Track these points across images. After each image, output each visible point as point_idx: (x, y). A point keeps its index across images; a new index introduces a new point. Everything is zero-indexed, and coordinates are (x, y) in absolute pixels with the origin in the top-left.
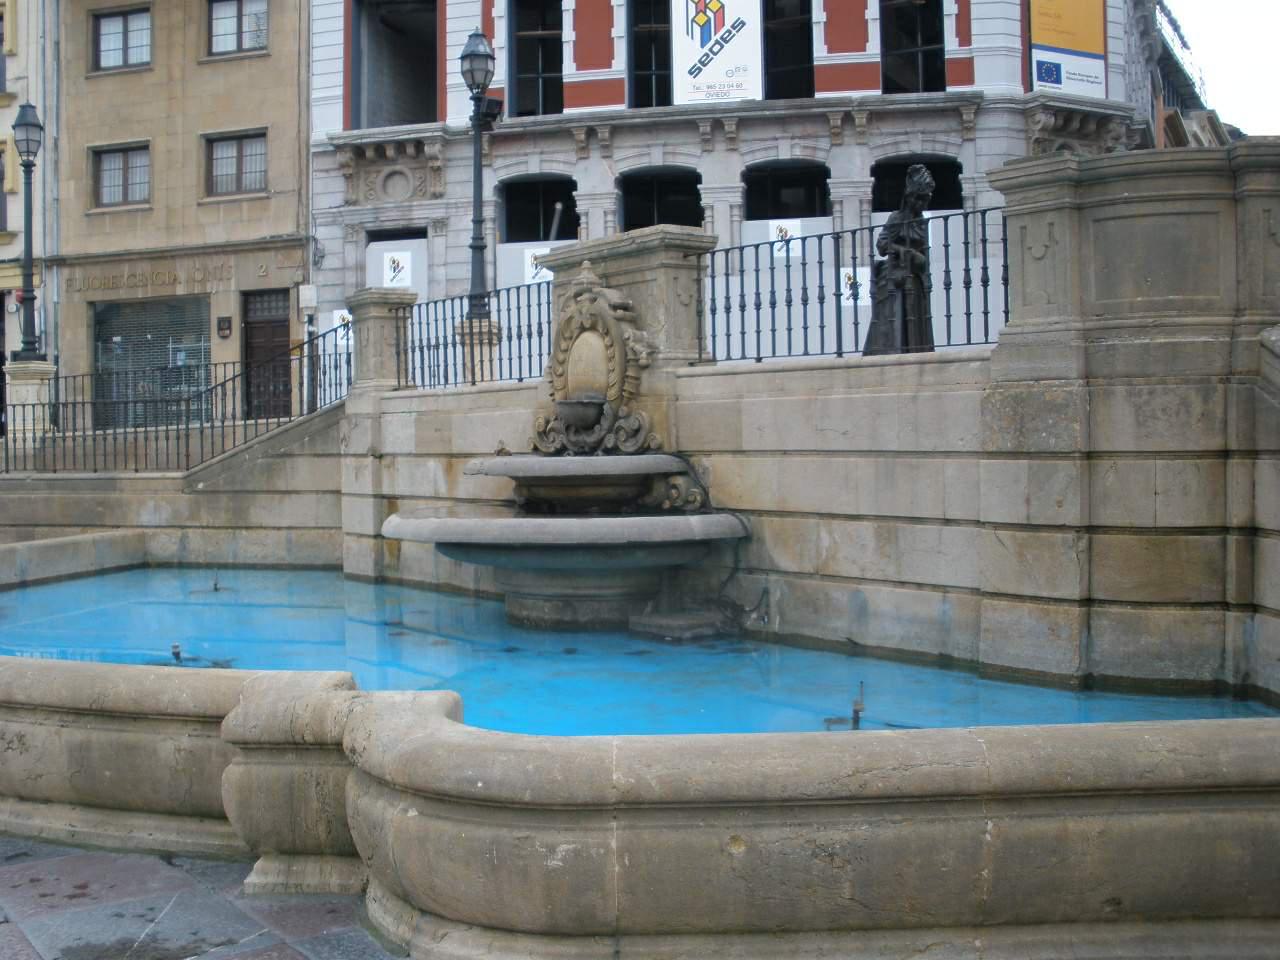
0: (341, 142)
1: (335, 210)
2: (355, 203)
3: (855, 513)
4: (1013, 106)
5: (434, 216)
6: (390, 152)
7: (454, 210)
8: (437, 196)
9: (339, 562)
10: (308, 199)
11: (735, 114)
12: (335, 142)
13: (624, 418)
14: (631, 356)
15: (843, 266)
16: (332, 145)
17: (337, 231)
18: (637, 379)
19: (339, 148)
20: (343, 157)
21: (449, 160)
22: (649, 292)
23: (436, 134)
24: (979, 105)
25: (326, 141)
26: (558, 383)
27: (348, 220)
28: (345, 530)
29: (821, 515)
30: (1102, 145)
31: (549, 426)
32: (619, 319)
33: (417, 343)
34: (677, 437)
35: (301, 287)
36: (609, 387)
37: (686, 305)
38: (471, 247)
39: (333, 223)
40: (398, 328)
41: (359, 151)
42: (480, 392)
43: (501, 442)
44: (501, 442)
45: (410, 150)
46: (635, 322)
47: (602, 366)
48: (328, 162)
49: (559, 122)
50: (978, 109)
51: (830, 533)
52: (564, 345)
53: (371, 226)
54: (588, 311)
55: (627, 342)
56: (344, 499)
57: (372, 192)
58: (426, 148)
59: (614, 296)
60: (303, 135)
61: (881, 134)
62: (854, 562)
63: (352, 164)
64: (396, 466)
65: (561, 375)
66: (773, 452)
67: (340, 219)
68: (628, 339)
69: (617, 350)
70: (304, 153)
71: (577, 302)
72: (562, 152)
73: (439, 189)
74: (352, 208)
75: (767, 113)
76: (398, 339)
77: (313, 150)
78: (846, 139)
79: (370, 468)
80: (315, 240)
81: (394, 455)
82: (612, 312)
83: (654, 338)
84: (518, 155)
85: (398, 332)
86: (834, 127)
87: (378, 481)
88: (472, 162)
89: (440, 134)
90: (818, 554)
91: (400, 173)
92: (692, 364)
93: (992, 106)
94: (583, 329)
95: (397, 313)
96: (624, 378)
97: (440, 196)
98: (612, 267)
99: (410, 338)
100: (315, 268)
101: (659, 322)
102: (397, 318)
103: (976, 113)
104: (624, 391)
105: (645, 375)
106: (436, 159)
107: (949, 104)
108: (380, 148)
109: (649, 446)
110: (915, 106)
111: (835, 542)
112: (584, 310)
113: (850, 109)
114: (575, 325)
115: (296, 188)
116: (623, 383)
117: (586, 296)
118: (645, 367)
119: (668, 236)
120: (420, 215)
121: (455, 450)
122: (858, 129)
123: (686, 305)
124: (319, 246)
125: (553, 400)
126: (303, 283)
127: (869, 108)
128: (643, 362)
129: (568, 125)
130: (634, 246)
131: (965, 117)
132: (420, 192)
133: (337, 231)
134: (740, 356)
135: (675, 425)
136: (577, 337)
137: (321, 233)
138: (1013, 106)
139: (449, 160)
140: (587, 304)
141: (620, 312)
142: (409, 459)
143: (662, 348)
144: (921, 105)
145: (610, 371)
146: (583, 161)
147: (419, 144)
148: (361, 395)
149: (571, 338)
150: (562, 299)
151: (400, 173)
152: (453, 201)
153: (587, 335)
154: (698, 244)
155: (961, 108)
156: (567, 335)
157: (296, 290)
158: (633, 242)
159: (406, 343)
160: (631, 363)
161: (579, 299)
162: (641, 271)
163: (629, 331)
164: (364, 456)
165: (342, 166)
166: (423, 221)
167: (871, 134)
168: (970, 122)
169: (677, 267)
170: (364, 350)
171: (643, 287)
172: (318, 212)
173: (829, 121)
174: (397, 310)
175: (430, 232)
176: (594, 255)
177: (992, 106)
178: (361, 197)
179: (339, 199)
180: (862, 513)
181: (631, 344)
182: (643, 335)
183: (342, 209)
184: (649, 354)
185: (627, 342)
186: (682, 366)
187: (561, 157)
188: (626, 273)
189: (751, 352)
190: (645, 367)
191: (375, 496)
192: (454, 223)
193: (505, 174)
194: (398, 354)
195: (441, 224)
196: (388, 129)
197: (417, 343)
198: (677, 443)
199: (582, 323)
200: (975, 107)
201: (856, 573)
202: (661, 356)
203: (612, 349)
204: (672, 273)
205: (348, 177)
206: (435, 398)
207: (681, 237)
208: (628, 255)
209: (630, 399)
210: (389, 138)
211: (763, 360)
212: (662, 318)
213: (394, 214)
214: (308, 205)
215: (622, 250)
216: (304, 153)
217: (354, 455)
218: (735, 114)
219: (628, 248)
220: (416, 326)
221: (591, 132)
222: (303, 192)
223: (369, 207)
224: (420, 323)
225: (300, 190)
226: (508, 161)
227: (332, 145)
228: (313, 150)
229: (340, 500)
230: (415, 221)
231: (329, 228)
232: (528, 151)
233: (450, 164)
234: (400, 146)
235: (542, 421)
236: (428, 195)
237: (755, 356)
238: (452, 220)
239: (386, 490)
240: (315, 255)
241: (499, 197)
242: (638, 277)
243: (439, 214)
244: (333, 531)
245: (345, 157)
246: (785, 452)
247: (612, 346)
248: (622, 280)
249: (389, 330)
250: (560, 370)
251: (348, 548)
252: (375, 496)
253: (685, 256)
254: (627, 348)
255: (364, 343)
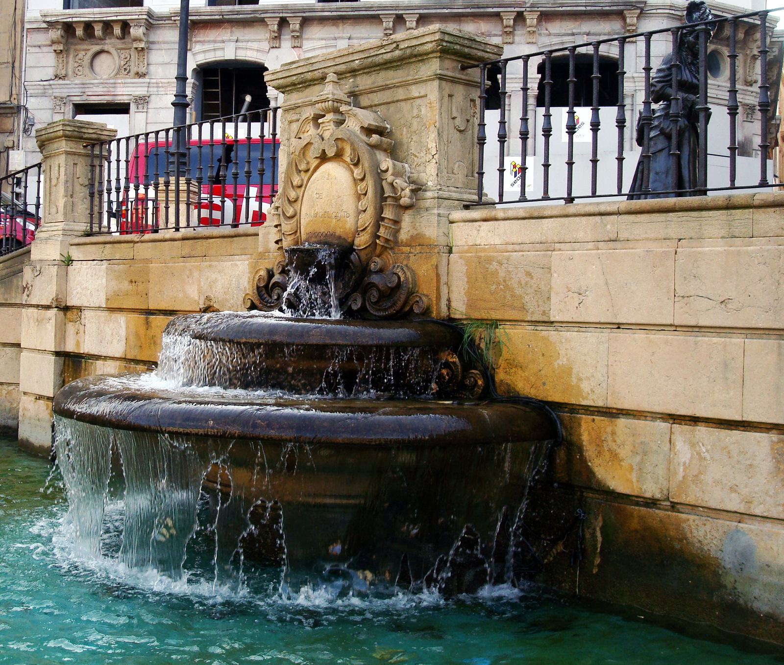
0: (53, 19)
1: (45, 83)
2: (64, 77)
3: (738, 418)
4: (673, 12)
5: (137, 93)
6: (98, 31)
7: (155, 89)
8: (140, 75)
9: (10, 423)
10: (21, 71)
11: (416, 11)
12: (48, 19)
13: (377, 272)
14: (388, 192)
15: (508, 155)
16: (45, 22)
17: (46, 103)
18: (396, 222)
19: (51, 25)
20: (55, 34)
21: (153, 43)
22: (415, 112)
23: (141, 17)
24: (642, 9)
25: (40, 18)
26: (287, 227)
27: (58, 92)
28: (22, 388)
29: (675, 418)
30: (748, 52)
31: (273, 281)
32: (374, 147)
33: (114, 184)
34: (449, 300)
35: (11, 152)
36: (357, 232)
37: (460, 131)
38: (173, 104)
39: (43, 95)
40: (93, 166)
41: (68, 28)
42: (184, 239)
43: (208, 298)
44: (208, 298)
45: (117, 30)
46: (393, 152)
47: (349, 205)
48: (42, 38)
49: (255, 11)
50: (641, 13)
51: (693, 445)
52: (296, 181)
53: (78, 100)
54: (332, 135)
55: (385, 176)
56: (24, 354)
57: (80, 68)
58: (132, 30)
59: (368, 118)
60: (19, 12)
61: (550, 35)
62: (733, 489)
63: (63, 41)
64: (83, 321)
65: (292, 217)
66: (600, 325)
67: (50, 91)
68: (387, 171)
69: (370, 184)
70: (19, 29)
71: (317, 126)
72: (255, 41)
73: (143, 70)
74: (61, 82)
75: (446, 11)
76: (92, 179)
77: (27, 26)
78: (517, 39)
79: (53, 321)
80: (26, 109)
81: (80, 309)
82: (364, 138)
83: (419, 172)
84: (215, 42)
85: (92, 171)
86: (507, 27)
87: (61, 334)
88: (177, 46)
89: (145, 17)
90: (670, 471)
91: (108, 52)
92: (466, 207)
93: (654, 11)
94: (323, 158)
95: (93, 151)
96: (379, 219)
97: (143, 75)
98: (364, 82)
99: (106, 178)
100: (25, 135)
101: (428, 150)
102: (93, 156)
103: (638, 18)
104: (378, 237)
105: (407, 219)
106: (140, 40)
107: (615, 8)
108: (88, 26)
109: (411, 309)
110: (584, 8)
111: (702, 459)
112: (327, 135)
113: (523, 9)
114: (313, 153)
115: (10, 60)
116: (378, 228)
117: (330, 116)
118: (407, 208)
119: (447, 38)
120: (124, 92)
121: (152, 306)
122: (529, 29)
123: (460, 131)
124: (29, 115)
125: (281, 248)
126: (13, 148)
127: (540, 9)
128: (405, 201)
129: (263, 16)
130: (397, 53)
131: (628, 21)
132: (124, 70)
133: (46, 103)
134: (540, 195)
135: (447, 284)
136: (317, 168)
137: (32, 104)
138: (673, 12)
139: (153, 43)
140: (332, 126)
141: (375, 138)
142: (99, 313)
143: (430, 183)
144: (588, 8)
145: (359, 212)
146: (275, 50)
147: (125, 26)
148: (47, 239)
149: (307, 171)
150: (295, 126)
151: (108, 52)
152: (154, 81)
153: (328, 167)
154: (480, 54)
155: (625, 12)
156: (303, 167)
157: (5, 154)
158: (397, 47)
159: (101, 183)
160: (389, 201)
161: (320, 121)
162: (406, 85)
163: (386, 163)
164: (48, 307)
165: (53, 42)
166: (125, 98)
167: (540, 34)
168: (633, 25)
169: (453, 81)
170: (54, 189)
171: (405, 106)
172: (29, 83)
173: (502, 20)
174: (93, 146)
175: (133, 107)
176: (342, 68)
177: (654, 11)
178: (70, 73)
179: (50, 73)
180: (747, 418)
181: (389, 177)
182: (403, 167)
183: (51, 82)
184: (413, 191)
185: (385, 176)
186: (455, 208)
187: (255, 45)
188: (386, 88)
189: (558, 188)
190: (407, 208)
191: (57, 354)
192: (154, 102)
193: (202, 59)
194: (92, 195)
195: (143, 101)
196: (97, 10)
197: (114, 184)
198: (449, 307)
199: (324, 151)
200: (639, 11)
201: (734, 503)
202: (429, 194)
203: (364, 184)
204: (447, 87)
205: (58, 53)
206: (132, 244)
207: (461, 41)
208: (387, 65)
209: (384, 248)
210: (98, 17)
211: (576, 201)
212: (432, 145)
213: (99, 90)
214: (20, 77)
215: (378, 59)
216: (19, 29)
217: (37, 306)
218: (416, 11)
219: (388, 56)
220: (114, 165)
221: (283, 23)
222: (17, 64)
223: (77, 82)
224: (118, 161)
225: (13, 63)
226: (207, 47)
227: (45, 22)
228: (27, 26)
229: (18, 359)
230: (119, 98)
231: (39, 99)
232: (225, 38)
233: (152, 46)
234: (107, 26)
235: (263, 273)
236: (132, 73)
237: (566, 196)
238: (153, 98)
239: (70, 347)
240: (25, 123)
241: (196, 79)
242: (400, 94)
243: (141, 91)
244: (11, 388)
245: (55, 34)
246: (619, 326)
247: (362, 180)
248: (377, 98)
249: (82, 170)
250: (290, 212)
251: (24, 409)
252: (57, 354)
253: (463, 68)
254: (384, 183)
255: (54, 182)
